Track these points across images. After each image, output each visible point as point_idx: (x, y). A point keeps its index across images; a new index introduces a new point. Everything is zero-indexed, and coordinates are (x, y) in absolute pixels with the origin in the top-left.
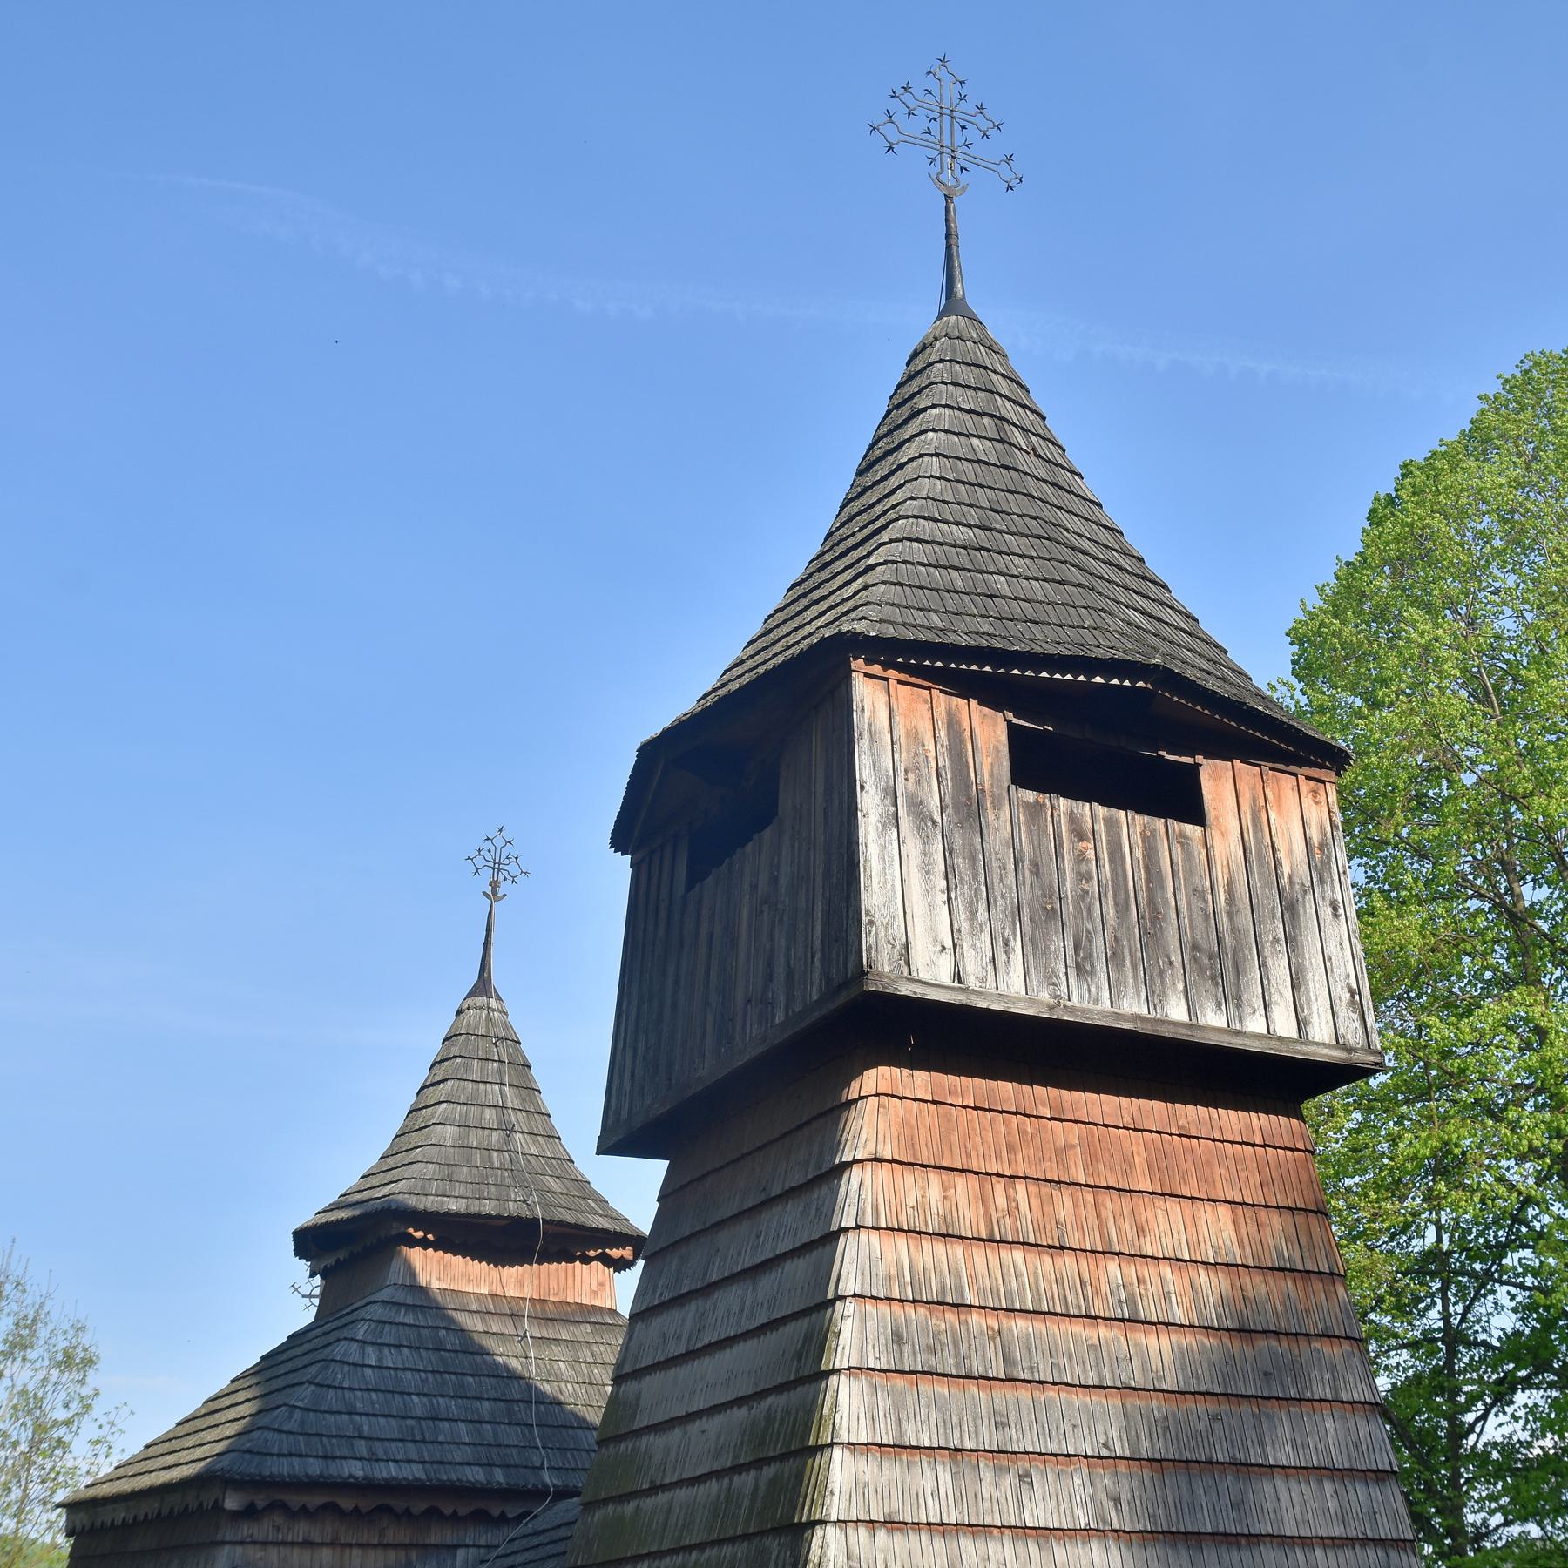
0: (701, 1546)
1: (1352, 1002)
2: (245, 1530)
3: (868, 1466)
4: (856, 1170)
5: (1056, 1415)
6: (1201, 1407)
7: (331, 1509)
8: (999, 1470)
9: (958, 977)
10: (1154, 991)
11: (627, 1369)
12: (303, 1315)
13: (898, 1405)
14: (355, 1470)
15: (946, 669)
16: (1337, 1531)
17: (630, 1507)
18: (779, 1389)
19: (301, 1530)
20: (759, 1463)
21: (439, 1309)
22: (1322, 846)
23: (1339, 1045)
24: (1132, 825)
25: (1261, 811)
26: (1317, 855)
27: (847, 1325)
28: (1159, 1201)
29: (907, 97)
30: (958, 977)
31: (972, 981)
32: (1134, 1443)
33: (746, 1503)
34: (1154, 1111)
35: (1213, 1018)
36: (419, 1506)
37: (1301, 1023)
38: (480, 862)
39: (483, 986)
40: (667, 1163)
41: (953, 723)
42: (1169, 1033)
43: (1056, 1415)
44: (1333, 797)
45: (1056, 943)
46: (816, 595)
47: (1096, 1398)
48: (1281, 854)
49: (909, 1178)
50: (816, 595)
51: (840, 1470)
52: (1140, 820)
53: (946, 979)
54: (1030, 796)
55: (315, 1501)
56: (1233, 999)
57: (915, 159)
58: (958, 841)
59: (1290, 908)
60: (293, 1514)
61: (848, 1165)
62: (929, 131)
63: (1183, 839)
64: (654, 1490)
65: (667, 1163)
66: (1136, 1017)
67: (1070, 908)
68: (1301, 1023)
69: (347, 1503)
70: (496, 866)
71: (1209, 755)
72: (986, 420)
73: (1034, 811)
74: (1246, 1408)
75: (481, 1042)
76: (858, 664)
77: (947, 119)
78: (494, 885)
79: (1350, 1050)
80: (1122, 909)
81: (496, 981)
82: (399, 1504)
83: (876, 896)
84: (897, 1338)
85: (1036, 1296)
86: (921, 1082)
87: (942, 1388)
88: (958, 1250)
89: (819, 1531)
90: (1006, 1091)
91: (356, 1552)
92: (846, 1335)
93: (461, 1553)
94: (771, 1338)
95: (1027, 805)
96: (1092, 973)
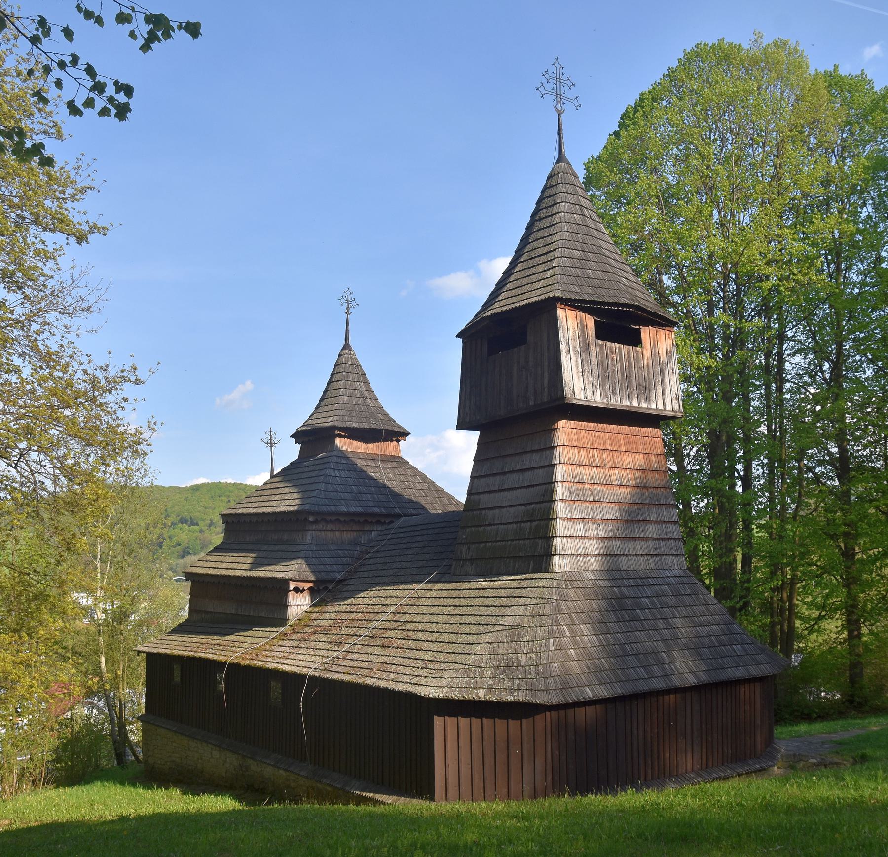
0: (512, 540)
1: (676, 398)
2: (315, 527)
3: (566, 523)
4: (558, 448)
5: (604, 510)
6: (636, 507)
7: (338, 520)
8: (593, 523)
9: (586, 397)
10: (630, 400)
11: (473, 492)
12: (295, 456)
13: (571, 509)
14: (344, 509)
15: (581, 306)
16: (665, 536)
17: (481, 529)
18: (537, 503)
19: (330, 527)
20: (531, 521)
21: (347, 458)
22: (670, 351)
23: (673, 411)
24: (625, 348)
25: (656, 341)
26: (669, 355)
27: (559, 488)
28: (627, 453)
29: (547, 75)
30: (586, 397)
31: (589, 398)
32: (621, 516)
33: (528, 530)
34: (625, 429)
35: (644, 405)
36: (362, 520)
37: (664, 405)
38: (343, 300)
39: (347, 346)
40: (479, 433)
41: (581, 318)
42: (634, 410)
43: (604, 510)
44: (674, 336)
45: (607, 386)
46: (533, 270)
47: (613, 505)
48: (661, 355)
49: (571, 450)
50: (533, 270)
51: (559, 524)
52: (627, 347)
53: (583, 398)
54: (600, 342)
55: (334, 518)
56: (648, 400)
57: (549, 98)
58: (584, 357)
59: (662, 371)
60: (327, 522)
61: (556, 447)
62: (553, 89)
63: (637, 351)
64: (490, 525)
65: (479, 433)
66: (626, 406)
67: (610, 375)
68: (664, 405)
69: (342, 519)
70: (348, 302)
71: (644, 326)
72: (577, 206)
73: (601, 346)
74: (646, 507)
75: (351, 367)
76: (558, 305)
77: (558, 83)
78: (348, 309)
79: (675, 412)
80: (622, 374)
81: (351, 343)
82: (356, 519)
83: (567, 375)
84: (570, 492)
85: (600, 480)
86: (572, 423)
87: (580, 504)
88: (582, 468)
89: (555, 539)
90: (591, 425)
91: (345, 532)
92: (558, 491)
93: (373, 533)
94: (532, 489)
95: (600, 345)
96: (616, 394)
